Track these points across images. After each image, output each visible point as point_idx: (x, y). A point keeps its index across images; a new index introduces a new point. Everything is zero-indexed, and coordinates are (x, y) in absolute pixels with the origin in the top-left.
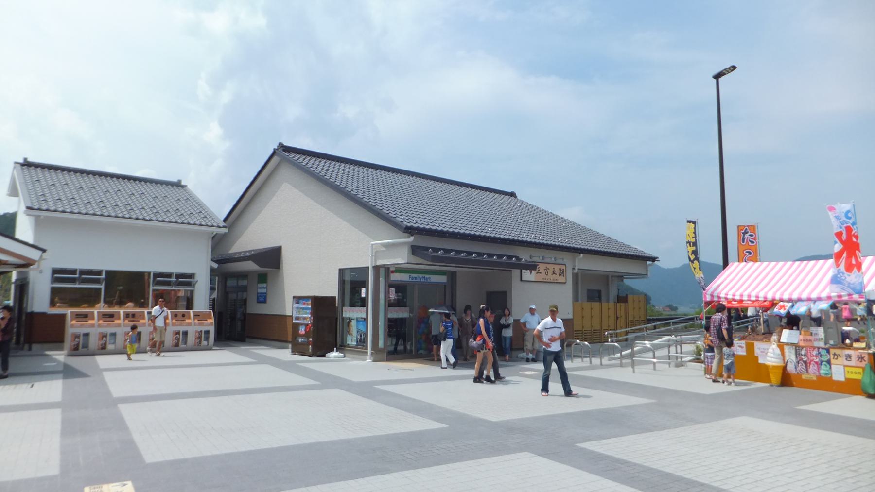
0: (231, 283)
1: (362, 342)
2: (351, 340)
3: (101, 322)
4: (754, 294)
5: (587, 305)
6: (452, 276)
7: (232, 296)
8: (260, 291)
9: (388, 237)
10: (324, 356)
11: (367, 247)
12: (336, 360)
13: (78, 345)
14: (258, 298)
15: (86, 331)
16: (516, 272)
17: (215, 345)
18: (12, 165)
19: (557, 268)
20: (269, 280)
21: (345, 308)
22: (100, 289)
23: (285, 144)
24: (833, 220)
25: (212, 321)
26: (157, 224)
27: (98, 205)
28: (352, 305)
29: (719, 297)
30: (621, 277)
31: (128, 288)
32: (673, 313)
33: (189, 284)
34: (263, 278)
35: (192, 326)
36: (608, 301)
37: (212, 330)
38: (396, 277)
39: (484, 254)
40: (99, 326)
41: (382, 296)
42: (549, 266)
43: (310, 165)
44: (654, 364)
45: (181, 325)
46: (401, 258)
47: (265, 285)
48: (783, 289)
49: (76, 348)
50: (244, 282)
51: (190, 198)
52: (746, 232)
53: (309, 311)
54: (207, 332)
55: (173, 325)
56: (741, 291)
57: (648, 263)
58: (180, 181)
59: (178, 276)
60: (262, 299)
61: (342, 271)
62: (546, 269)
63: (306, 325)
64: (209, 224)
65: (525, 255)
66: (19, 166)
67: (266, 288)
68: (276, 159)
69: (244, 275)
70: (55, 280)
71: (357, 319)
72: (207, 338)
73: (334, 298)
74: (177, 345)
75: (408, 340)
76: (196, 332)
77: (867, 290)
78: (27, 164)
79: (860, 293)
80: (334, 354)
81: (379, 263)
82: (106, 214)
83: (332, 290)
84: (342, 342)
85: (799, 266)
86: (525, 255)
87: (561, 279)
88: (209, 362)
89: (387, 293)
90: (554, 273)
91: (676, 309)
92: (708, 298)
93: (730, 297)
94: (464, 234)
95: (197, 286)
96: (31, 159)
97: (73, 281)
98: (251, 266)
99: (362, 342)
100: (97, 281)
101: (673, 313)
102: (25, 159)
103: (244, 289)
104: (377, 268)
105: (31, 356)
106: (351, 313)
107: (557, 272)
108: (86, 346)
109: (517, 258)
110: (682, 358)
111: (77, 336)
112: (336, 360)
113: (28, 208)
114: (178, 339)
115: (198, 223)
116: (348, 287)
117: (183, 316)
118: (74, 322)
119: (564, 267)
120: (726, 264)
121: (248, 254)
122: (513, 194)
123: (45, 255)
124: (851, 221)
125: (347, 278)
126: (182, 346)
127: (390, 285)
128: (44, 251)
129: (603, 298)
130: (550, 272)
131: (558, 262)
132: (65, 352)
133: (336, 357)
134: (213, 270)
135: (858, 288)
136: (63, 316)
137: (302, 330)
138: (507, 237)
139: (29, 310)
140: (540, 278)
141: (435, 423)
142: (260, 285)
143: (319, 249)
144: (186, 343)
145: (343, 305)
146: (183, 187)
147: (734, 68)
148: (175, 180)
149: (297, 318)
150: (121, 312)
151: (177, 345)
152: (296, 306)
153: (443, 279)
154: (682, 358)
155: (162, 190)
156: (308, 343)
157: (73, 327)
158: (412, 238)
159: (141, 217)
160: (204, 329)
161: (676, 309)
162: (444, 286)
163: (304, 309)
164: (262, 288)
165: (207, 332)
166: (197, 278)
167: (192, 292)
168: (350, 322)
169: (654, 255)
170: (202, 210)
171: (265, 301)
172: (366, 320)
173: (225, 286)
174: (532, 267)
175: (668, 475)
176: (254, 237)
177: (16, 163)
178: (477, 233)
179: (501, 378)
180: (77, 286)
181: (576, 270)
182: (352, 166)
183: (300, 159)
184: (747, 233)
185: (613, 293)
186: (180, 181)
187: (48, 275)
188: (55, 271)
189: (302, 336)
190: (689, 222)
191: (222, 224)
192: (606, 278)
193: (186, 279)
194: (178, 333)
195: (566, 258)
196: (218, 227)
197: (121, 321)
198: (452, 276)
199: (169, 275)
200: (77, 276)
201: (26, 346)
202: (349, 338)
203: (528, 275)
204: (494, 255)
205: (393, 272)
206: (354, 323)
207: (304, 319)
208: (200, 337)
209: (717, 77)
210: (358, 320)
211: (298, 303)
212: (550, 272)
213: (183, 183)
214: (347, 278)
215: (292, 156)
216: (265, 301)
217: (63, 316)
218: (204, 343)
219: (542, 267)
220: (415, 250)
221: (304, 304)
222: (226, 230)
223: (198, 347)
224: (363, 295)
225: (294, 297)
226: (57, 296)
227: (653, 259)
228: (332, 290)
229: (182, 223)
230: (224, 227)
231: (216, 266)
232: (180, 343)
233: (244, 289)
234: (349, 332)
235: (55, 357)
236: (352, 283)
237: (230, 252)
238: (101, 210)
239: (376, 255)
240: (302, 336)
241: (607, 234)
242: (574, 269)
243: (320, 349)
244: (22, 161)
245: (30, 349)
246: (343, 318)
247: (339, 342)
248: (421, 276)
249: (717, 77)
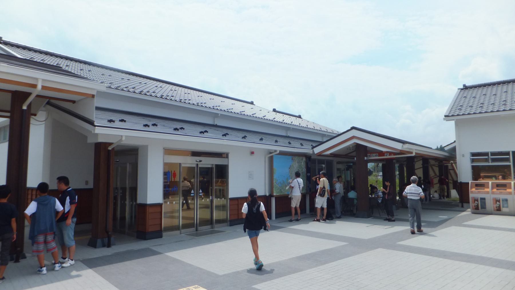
3: (495, 190)
15: (483, 196)
40: (493, 193)
49: (477, 208)
70: (473, 161)
78: (466, 88)
96: (468, 84)
97: (486, 160)
100: (508, 160)
102: (464, 85)
108: (484, 206)
111: (476, 200)
126: (480, 210)
141: (299, 228)
179: (422, 231)
187: (468, 157)
188: (473, 154)
197: (489, 190)
244: (462, 87)
245: (462, 206)
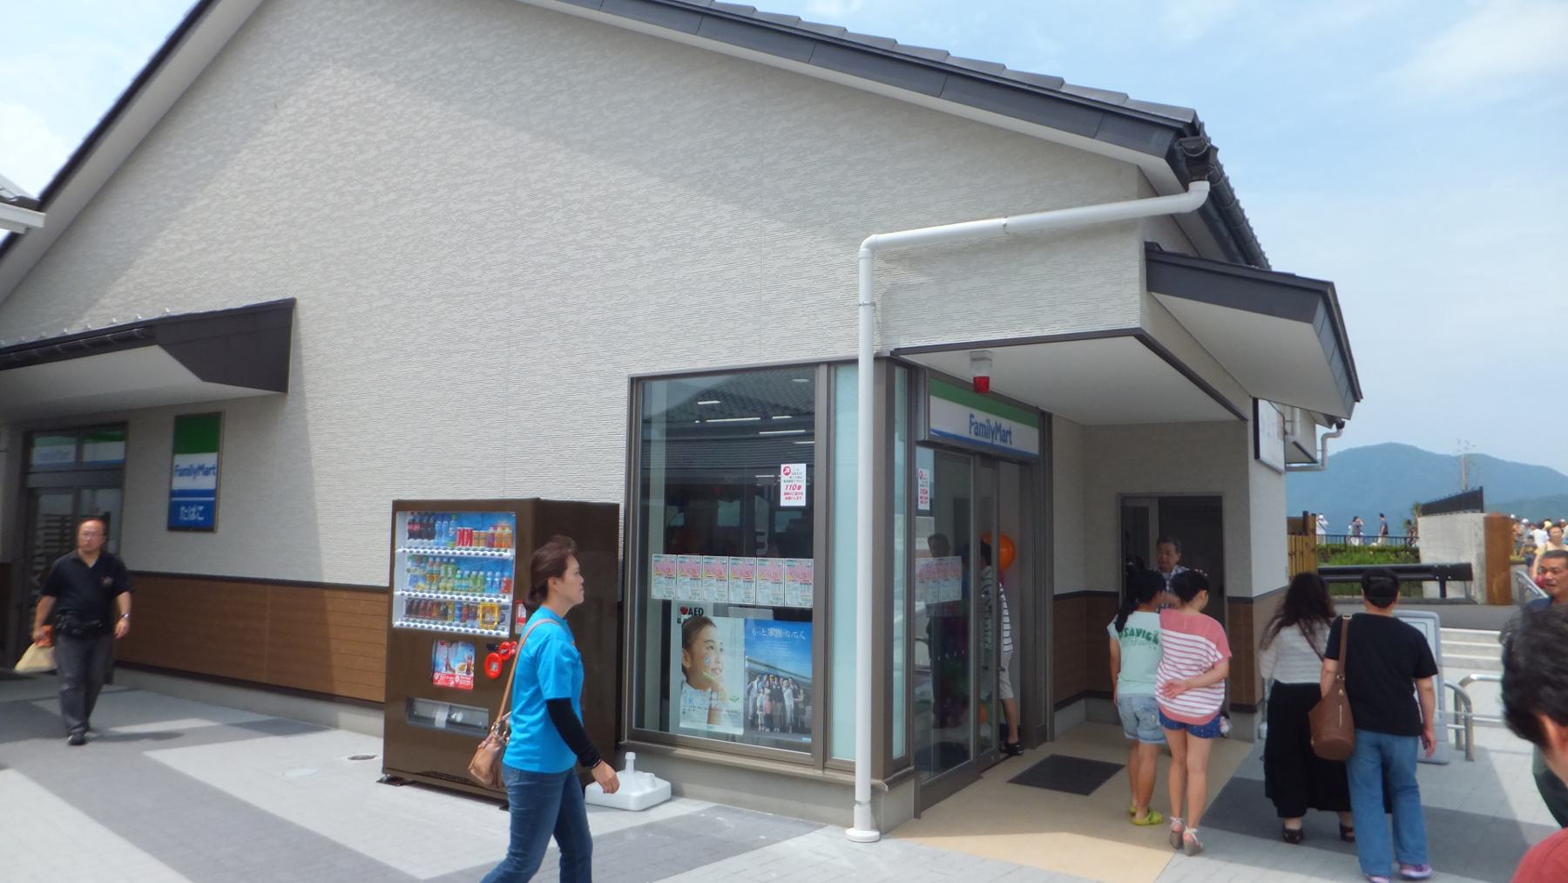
0: (49, 453)
8: (181, 483)
14: (174, 510)
20: (231, 438)
21: (660, 561)
33: (1143, 513)
34: (198, 429)
47: (209, 459)
50: (110, 451)
53: (510, 574)
60: (195, 515)
61: (638, 384)
67: (217, 471)
73: (617, 506)
83: (597, 473)
84: (664, 722)
89: (821, 487)
98: (159, 374)
99: (799, 723)
104: (904, 375)
125: (659, 403)
142: (184, 461)
152: (408, 547)
163: (459, 561)
164: (193, 473)
171: (207, 524)
173: (25, 468)
176: (178, 258)
206: (724, 634)
207: (468, 612)
211: (423, 531)
216: (207, 524)
225: (399, 506)
233: (113, 476)
235: (41, 704)
239: (885, 307)
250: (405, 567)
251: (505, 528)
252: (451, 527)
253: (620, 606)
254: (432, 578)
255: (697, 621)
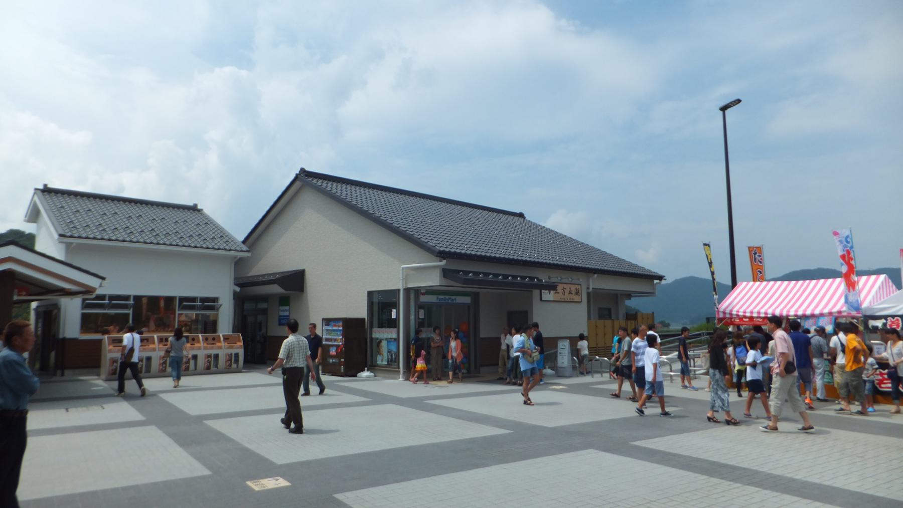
0: (248, 306)
1: (393, 361)
2: (382, 360)
4: (763, 311)
5: (601, 323)
6: (476, 297)
7: (250, 319)
8: (281, 314)
9: (417, 261)
10: (355, 376)
11: (396, 270)
12: (367, 379)
13: (116, 369)
14: (280, 320)
16: (536, 292)
17: (244, 367)
18: (32, 192)
19: (573, 288)
21: (375, 329)
22: (128, 315)
23: (307, 169)
24: (838, 244)
25: (241, 344)
26: (183, 249)
27: (97, 228)
28: (381, 326)
29: (731, 314)
30: (629, 295)
31: (150, 313)
32: (665, 329)
33: (212, 308)
34: (284, 301)
35: (223, 350)
36: (618, 319)
37: (241, 352)
38: (424, 299)
39: (480, 273)
41: (412, 317)
42: (565, 286)
43: (329, 189)
44: (671, 376)
45: (212, 348)
46: (433, 280)
47: (287, 308)
48: (790, 305)
50: (264, 305)
51: (208, 222)
52: (755, 254)
53: (340, 333)
54: (237, 355)
55: (205, 348)
56: (744, 308)
57: (656, 281)
58: (196, 205)
59: (203, 300)
61: (370, 294)
62: (564, 289)
63: (337, 346)
64: (161, 242)
65: (544, 277)
66: (39, 192)
67: (289, 310)
68: (298, 184)
69: (265, 298)
71: (386, 339)
72: (237, 361)
74: (208, 368)
75: (427, 360)
76: (227, 354)
77: (865, 305)
78: (47, 191)
79: (858, 309)
80: (365, 374)
81: (410, 285)
82: (76, 235)
83: (361, 311)
85: (802, 285)
86: (544, 277)
87: (577, 298)
88: (263, 383)
89: (398, 314)
90: (570, 293)
91: (668, 325)
92: (721, 315)
93: (741, 314)
94: (470, 255)
95: (221, 309)
96: (50, 186)
98: (276, 289)
100: (125, 307)
101: (665, 329)
102: (45, 186)
103: (265, 312)
104: (407, 290)
105: (64, 381)
106: (380, 334)
107: (573, 292)
109: (538, 279)
110: (695, 371)
112: (367, 379)
113: (61, 235)
114: (210, 363)
115: (148, 241)
116: (376, 308)
117: (193, 339)
118: (111, 347)
119: (579, 287)
120: (734, 284)
121: (272, 278)
122: (521, 215)
123: (104, 282)
124: (849, 245)
125: (375, 300)
126: (213, 369)
127: (420, 306)
128: (103, 279)
129: (613, 317)
130: (567, 291)
131: (575, 281)
132: (103, 376)
133: (367, 377)
134: (235, 293)
135: (856, 305)
136: (100, 342)
137: (333, 351)
138: (502, 256)
139: (61, 336)
140: (558, 297)
142: (282, 308)
143: (345, 274)
144: (216, 366)
145: (372, 327)
146: (199, 211)
147: (739, 101)
148: (191, 204)
149: (327, 340)
150: (155, 336)
151: (208, 368)
152: (325, 328)
153: (467, 300)
154: (695, 371)
155: (182, 215)
156: (340, 364)
157: (111, 353)
158: (444, 262)
159: (113, 238)
160: (234, 351)
161: (668, 325)
162: (468, 306)
163: (334, 330)
164: (284, 311)
165: (237, 355)
166: (221, 302)
167: (217, 315)
168: (380, 342)
169: (661, 273)
170: (223, 235)
172: (397, 340)
174: (552, 287)
175: (714, 463)
176: (279, 257)
177: (36, 189)
178: (473, 253)
180: (106, 311)
181: (591, 290)
182: (344, 186)
183: (329, 186)
184: (755, 253)
185: (622, 312)
186: (196, 205)
189: (333, 357)
190: (705, 245)
191: (245, 248)
192: (617, 297)
193: (210, 303)
194: (209, 356)
195: (581, 279)
196: (242, 251)
198: (476, 297)
199: (193, 299)
200: (107, 302)
201: (59, 372)
202: (379, 358)
203: (548, 295)
204: (526, 277)
205: (423, 294)
206: (384, 343)
207: (335, 340)
208: (230, 360)
209: (724, 109)
210: (389, 341)
211: (328, 325)
212: (567, 291)
213: (199, 207)
214: (375, 300)
215: (315, 181)
217: (100, 342)
218: (234, 366)
219: (560, 288)
220: (446, 273)
221: (335, 326)
222: (248, 254)
223: (228, 370)
224: (394, 316)
225: (323, 319)
226: (87, 322)
227: (661, 278)
228: (361, 311)
229: (158, 244)
230: (247, 251)
231: (238, 289)
232: (212, 367)
233: (265, 312)
234: (379, 353)
236: (382, 304)
237: (250, 275)
238: (71, 231)
239: (406, 279)
240: (333, 357)
241: (616, 254)
242: (588, 288)
243: (352, 371)
244: (41, 187)
245: (63, 375)
246: (372, 339)
247: (369, 363)
248: (447, 297)
249: (724, 109)
250: (324, 333)
251: (341, 324)
252: (331, 323)
253: (366, 340)
254: (329, 334)
255: (380, 342)
